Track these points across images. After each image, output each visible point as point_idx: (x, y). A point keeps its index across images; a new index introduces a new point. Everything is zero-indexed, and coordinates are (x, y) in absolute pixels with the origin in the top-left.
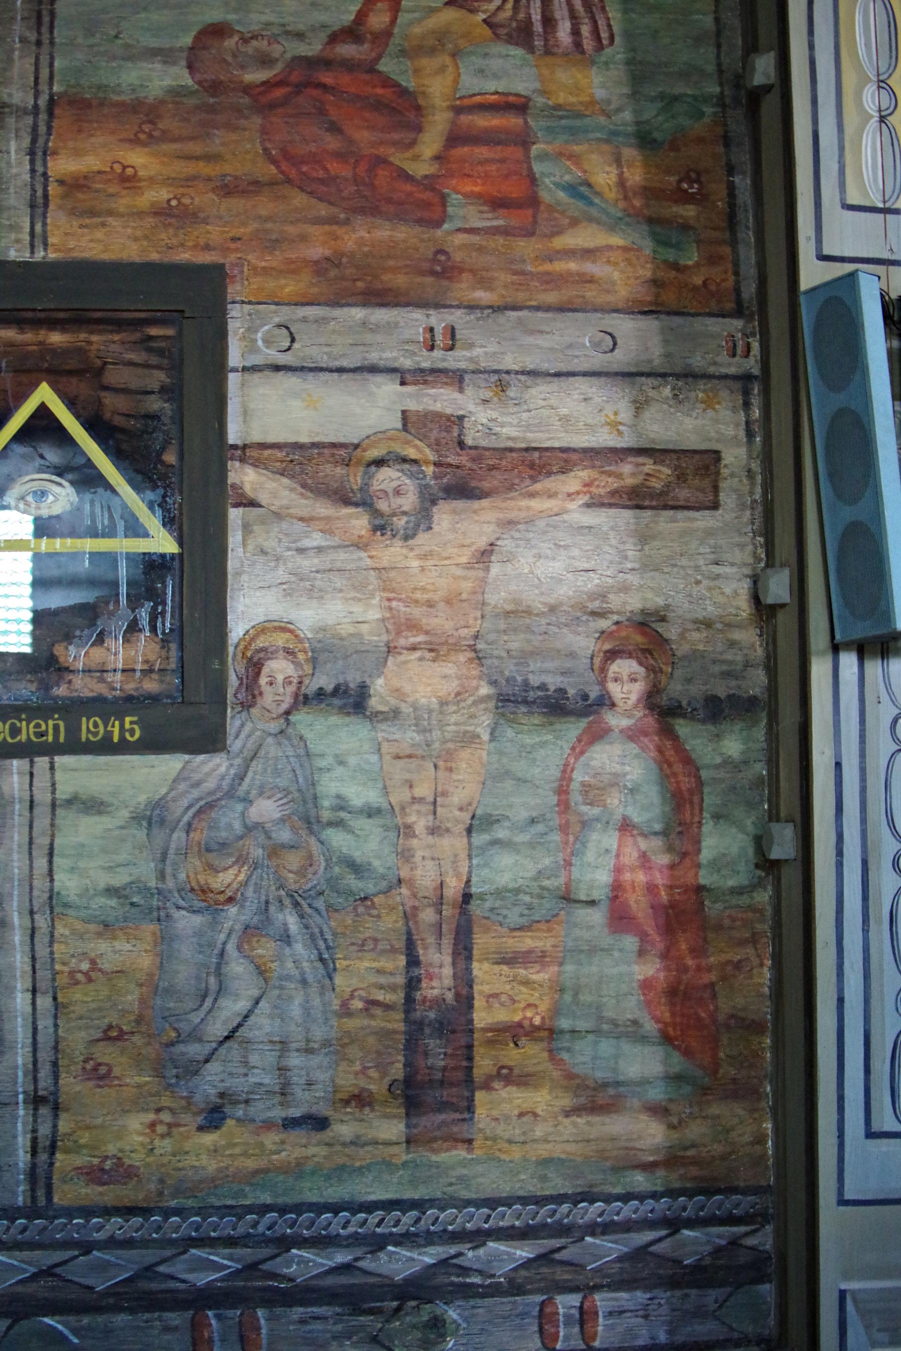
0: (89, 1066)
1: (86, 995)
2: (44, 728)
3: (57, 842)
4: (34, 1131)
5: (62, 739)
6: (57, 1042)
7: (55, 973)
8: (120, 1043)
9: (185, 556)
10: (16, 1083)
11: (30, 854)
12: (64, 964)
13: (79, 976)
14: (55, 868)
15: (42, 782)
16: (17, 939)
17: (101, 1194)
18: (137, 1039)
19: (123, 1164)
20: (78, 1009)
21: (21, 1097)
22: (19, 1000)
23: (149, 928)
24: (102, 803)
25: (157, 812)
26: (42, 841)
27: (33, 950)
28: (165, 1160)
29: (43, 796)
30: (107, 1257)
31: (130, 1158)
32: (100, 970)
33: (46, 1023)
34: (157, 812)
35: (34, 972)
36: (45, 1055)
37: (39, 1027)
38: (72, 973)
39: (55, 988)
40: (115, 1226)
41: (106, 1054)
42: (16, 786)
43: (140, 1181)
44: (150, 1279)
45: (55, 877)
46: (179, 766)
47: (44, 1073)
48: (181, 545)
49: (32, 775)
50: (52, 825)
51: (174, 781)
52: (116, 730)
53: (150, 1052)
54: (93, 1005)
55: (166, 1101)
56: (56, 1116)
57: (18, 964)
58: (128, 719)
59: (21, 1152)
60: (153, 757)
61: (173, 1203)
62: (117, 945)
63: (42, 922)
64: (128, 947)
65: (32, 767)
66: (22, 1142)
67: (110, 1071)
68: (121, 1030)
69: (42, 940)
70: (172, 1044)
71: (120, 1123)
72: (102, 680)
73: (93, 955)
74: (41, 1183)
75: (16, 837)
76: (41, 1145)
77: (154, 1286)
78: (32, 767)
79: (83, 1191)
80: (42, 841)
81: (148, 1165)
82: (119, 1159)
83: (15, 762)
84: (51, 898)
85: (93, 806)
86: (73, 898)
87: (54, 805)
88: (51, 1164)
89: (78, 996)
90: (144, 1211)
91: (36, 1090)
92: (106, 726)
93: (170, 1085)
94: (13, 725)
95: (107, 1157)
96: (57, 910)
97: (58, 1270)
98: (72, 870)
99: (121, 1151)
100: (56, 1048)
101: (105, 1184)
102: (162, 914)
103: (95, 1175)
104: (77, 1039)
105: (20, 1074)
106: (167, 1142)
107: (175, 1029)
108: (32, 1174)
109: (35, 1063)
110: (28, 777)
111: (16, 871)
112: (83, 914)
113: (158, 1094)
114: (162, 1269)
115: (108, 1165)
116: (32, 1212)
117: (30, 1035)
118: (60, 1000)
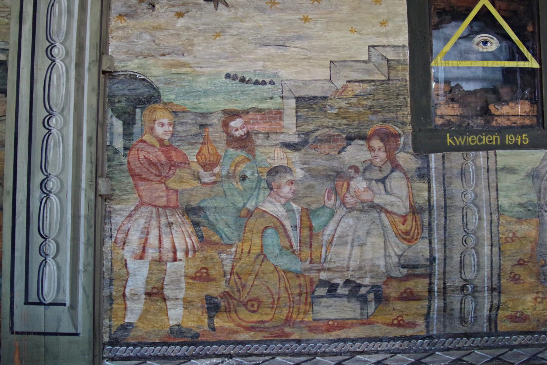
0: (512, 275)
1: (511, 247)
2: (492, 139)
3: (499, 185)
4: (492, 302)
5: (499, 144)
6: (500, 266)
7: (500, 238)
8: (523, 266)
9: (543, 69)
10: (484, 282)
11: (489, 190)
12: (503, 234)
13: (509, 239)
14: (499, 196)
15: (492, 161)
16: (485, 224)
17: (516, 326)
18: (530, 264)
19: (523, 314)
20: (508, 253)
21: (486, 288)
22: (486, 249)
23: (535, 221)
24: (514, 169)
25: (535, 173)
26: (493, 185)
27: (491, 229)
28: (539, 312)
29: (492, 167)
30: (519, 351)
31: (526, 312)
32: (517, 237)
33: (495, 258)
34: (535, 173)
35: (492, 238)
36: (495, 271)
37: (494, 260)
38: (506, 238)
39: (499, 244)
40: (522, 339)
41: (519, 270)
42: (482, 162)
43: (530, 321)
44: (536, 360)
45: (499, 199)
46: (543, 154)
47: (495, 278)
48: (540, 64)
49: (488, 158)
50: (497, 178)
51: (542, 160)
52: (519, 140)
53: (535, 269)
54: (514, 251)
55: (540, 289)
56: (500, 296)
57: (486, 235)
58: (524, 135)
59: (485, 310)
60: (533, 151)
61: (542, 329)
62: (523, 227)
63: (495, 217)
64: (527, 227)
65: (488, 154)
66: (487, 306)
67: (520, 277)
68: (524, 261)
69: (494, 224)
70: (543, 266)
71: (524, 298)
72: (509, 120)
73: (514, 231)
74: (493, 323)
75: (483, 183)
76: (494, 308)
77: (537, 362)
78: (488, 154)
79: (509, 325)
80: (493, 185)
81: (533, 314)
82: (522, 312)
83: (481, 153)
84: (498, 208)
85: (511, 170)
86: (506, 208)
87: (496, 170)
88: (497, 315)
89: (508, 247)
90: (532, 333)
91: (492, 286)
92: (515, 138)
93: (542, 282)
94: (480, 137)
95: (518, 312)
96: (501, 213)
97: (501, 357)
98: (506, 196)
99: (524, 309)
100: (500, 268)
101: (517, 322)
102: (540, 214)
103: (513, 319)
104: (508, 264)
105: (486, 279)
106: (541, 305)
107: (544, 260)
108: (490, 319)
109: (492, 275)
110: (486, 159)
111: (484, 197)
112: (510, 214)
113: (537, 286)
114: (539, 355)
115: (518, 315)
116: (489, 334)
117: (490, 263)
118: (501, 249)
